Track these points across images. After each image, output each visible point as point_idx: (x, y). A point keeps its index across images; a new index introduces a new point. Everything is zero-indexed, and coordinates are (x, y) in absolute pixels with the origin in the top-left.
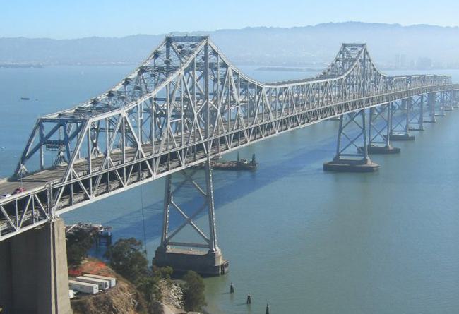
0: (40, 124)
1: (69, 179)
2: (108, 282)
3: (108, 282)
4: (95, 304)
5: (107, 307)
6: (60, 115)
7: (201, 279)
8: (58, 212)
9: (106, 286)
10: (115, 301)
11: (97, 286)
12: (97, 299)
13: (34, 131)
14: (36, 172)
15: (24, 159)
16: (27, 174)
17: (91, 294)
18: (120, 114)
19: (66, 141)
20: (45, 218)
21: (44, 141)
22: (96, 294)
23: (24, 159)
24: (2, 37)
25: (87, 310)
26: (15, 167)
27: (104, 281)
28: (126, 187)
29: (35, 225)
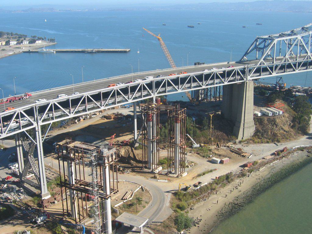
0: (256, 40)
1: (261, 64)
2: (278, 112)
3: (278, 112)
4: (267, 120)
5: (273, 123)
6: (269, 36)
7: (6, 41)
8: (250, 77)
9: (276, 114)
10: (277, 121)
11: (272, 113)
12: (269, 118)
13: (254, 42)
14: (253, 60)
15: (246, 54)
16: (247, 61)
17: (268, 116)
18: (297, 38)
19: (263, 49)
20: (243, 79)
21: (256, 47)
22: (270, 116)
23: (246, 54)
24: (1, 31)
25: (263, 122)
26: (241, 58)
27: (276, 111)
28: (297, 71)
29: (236, 82)
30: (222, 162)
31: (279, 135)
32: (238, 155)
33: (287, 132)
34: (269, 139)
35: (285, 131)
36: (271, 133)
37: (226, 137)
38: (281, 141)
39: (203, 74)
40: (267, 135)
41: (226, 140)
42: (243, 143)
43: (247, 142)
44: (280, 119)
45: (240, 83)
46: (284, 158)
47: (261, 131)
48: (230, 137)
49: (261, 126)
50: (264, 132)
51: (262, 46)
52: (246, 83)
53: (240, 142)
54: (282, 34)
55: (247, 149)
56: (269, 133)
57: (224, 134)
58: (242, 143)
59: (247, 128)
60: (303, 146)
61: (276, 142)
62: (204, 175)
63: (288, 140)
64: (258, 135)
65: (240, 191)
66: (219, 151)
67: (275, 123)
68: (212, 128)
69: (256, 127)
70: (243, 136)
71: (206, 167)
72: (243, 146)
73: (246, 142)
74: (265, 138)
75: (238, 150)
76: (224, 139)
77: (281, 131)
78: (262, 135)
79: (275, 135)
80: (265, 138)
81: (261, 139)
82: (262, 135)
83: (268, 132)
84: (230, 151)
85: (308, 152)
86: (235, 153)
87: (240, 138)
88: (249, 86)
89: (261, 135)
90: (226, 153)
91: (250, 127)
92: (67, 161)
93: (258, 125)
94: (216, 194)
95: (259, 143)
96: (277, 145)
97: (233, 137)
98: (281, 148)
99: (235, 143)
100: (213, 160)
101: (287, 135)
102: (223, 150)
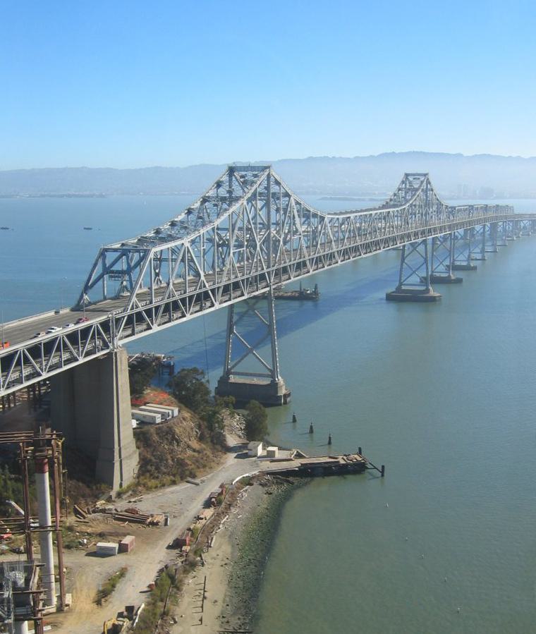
1: (132, 309)
3: (170, 412)
4: (157, 434)
5: (170, 437)
6: (123, 245)
10: (177, 431)
11: (160, 415)
12: (160, 428)
13: (97, 261)
15: (87, 288)
16: (90, 304)
17: (154, 423)
18: (183, 244)
19: (129, 271)
20: (108, 347)
21: (107, 271)
22: (158, 424)
23: (87, 288)
27: (167, 411)
28: (188, 317)
30: (123, 549)
31: (189, 462)
32: (140, 525)
33: (199, 452)
34: (174, 475)
35: (194, 451)
36: (173, 460)
37: (87, 491)
38: (197, 474)
39: (40, 344)
40: (166, 466)
41: (90, 496)
42: (126, 496)
43: (136, 488)
44: (180, 427)
45: (104, 355)
46: (233, 510)
47: (153, 458)
48: (94, 487)
49: (149, 450)
50: (158, 461)
51: (122, 265)
52: (116, 353)
53: (119, 495)
54: (142, 237)
55: (148, 504)
56: (170, 462)
57: (81, 484)
58: (124, 497)
59: (126, 457)
60: (247, 475)
61: (189, 479)
62: (115, 589)
63: (207, 469)
64: (149, 471)
65: (216, 601)
66: (90, 526)
67: (173, 438)
68: (64, 474)
69: (140, 454)
70: (122, 480)
71: (98, 569)
72: (130, 502)
73: (130, 492)
74: (164, 473)
75: (130, 515)
76: (83, 496)
77: (189, 452)
78: (157, 468)
79: (181, 463)
80: (164, 473)
81: (157, 478)
82: (157, 468)
83: (167, 460)
84: (114, 519)
85: (261, 485)
86: (130, 521)
87: (116, 487)
88: (121, 361)
89: (156, 469)
90: (109, 527)
91: (129, 457)
92: (65, 594)
93: (142, 449)
94: (175, 622)
95: (156, 487)
96: (197, 484)
97: (103, 486)
98: (213, 488)
99: (109, 500)
100: (101, 548)
101: (202, 458)
102: (97, 523)
